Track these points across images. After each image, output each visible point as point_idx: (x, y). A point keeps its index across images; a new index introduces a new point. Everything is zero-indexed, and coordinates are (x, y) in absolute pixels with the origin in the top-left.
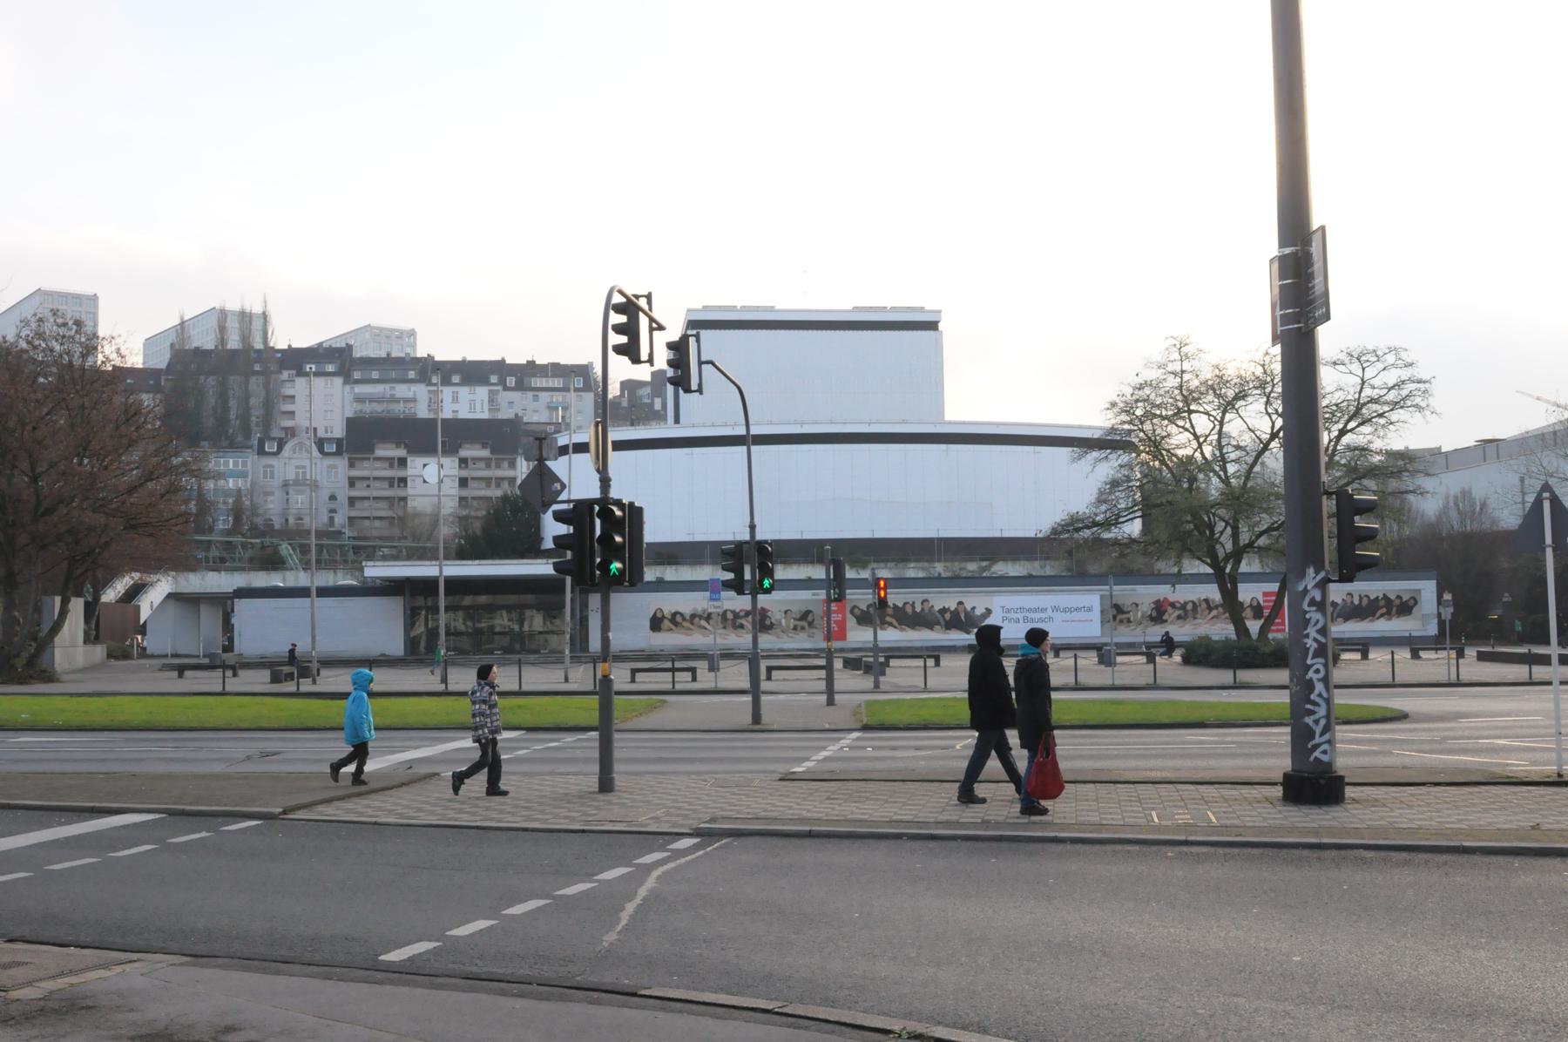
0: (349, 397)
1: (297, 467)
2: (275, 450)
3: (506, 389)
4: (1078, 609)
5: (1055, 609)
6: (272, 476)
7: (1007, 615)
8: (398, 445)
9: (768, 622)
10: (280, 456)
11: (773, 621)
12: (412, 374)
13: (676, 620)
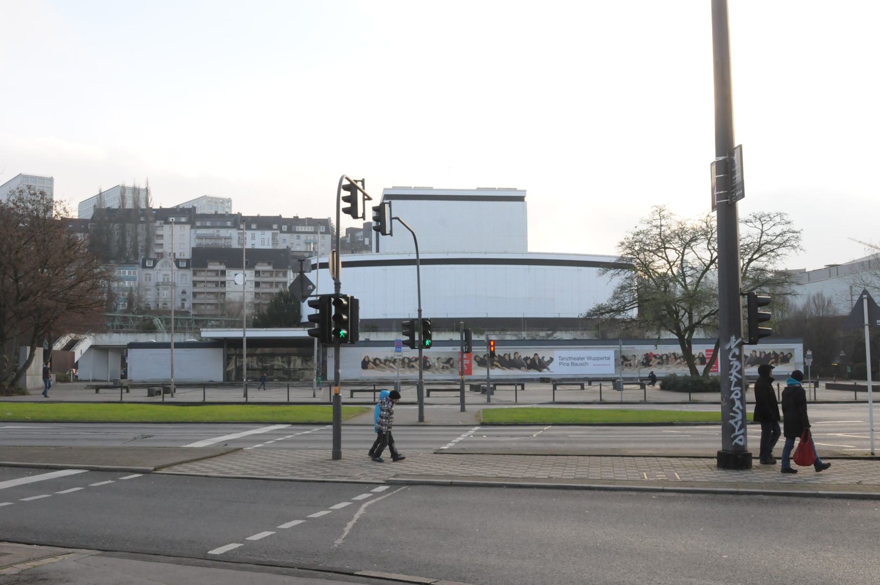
2: (152, 265)
3: (282, 232)
4: (601, 359)
5: (589, 358)
8: (221, 263)
9: (428, 364)
10: (154, 269)
12: (229, 224)
13: (376, 363)
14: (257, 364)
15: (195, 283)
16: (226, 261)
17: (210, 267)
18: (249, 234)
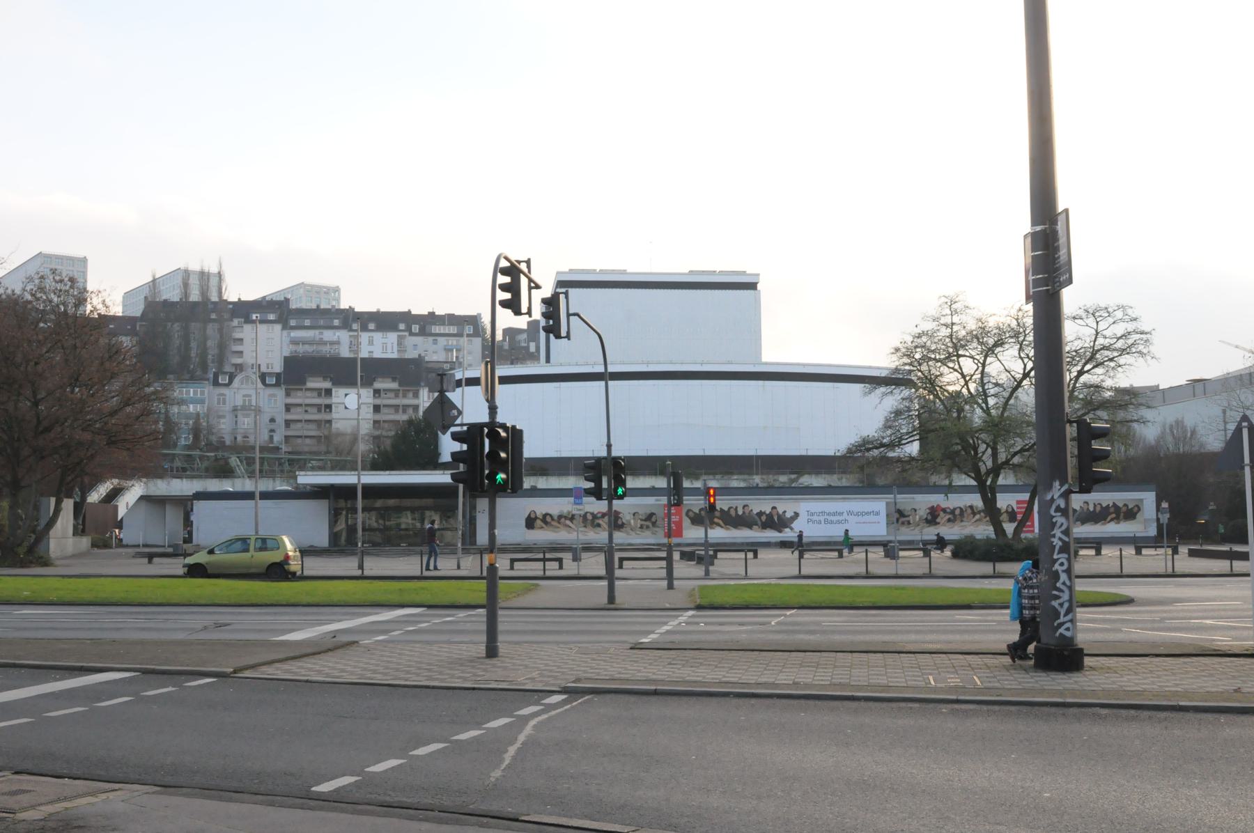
0: (286, 340)
1: (244, 396)
2: (227, 382)
3: (411, 334)
5: (850, 513)
6: (224, 403)
7: (812, 518)
8: (325, 378)
9: (620, 522)
10: (230, 387)
11: (624, 521)
12: (336, 323)
13: (547, 520)
15: (288, 408)
16: (332, 376)
17: (310, 385)
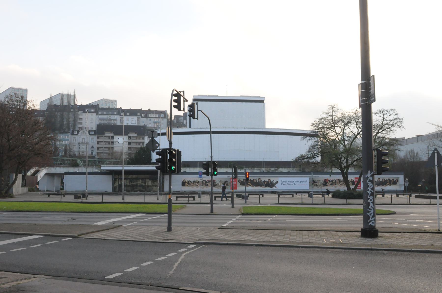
0: (98, 119)
1: (83, 138)
2: (77, 133)
3: (142, 117)
4: (302, 182)
5: (296, 181)
6: (75, 141)
7: (282, 183)
9: (215, 184)
10: (78, 135)
12: (115, 113)
13: (189, 183)
14: (129, 183)
15: (98, 143)
18: (125, 118)
